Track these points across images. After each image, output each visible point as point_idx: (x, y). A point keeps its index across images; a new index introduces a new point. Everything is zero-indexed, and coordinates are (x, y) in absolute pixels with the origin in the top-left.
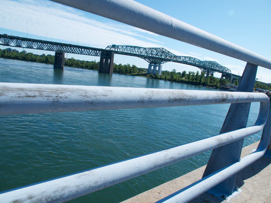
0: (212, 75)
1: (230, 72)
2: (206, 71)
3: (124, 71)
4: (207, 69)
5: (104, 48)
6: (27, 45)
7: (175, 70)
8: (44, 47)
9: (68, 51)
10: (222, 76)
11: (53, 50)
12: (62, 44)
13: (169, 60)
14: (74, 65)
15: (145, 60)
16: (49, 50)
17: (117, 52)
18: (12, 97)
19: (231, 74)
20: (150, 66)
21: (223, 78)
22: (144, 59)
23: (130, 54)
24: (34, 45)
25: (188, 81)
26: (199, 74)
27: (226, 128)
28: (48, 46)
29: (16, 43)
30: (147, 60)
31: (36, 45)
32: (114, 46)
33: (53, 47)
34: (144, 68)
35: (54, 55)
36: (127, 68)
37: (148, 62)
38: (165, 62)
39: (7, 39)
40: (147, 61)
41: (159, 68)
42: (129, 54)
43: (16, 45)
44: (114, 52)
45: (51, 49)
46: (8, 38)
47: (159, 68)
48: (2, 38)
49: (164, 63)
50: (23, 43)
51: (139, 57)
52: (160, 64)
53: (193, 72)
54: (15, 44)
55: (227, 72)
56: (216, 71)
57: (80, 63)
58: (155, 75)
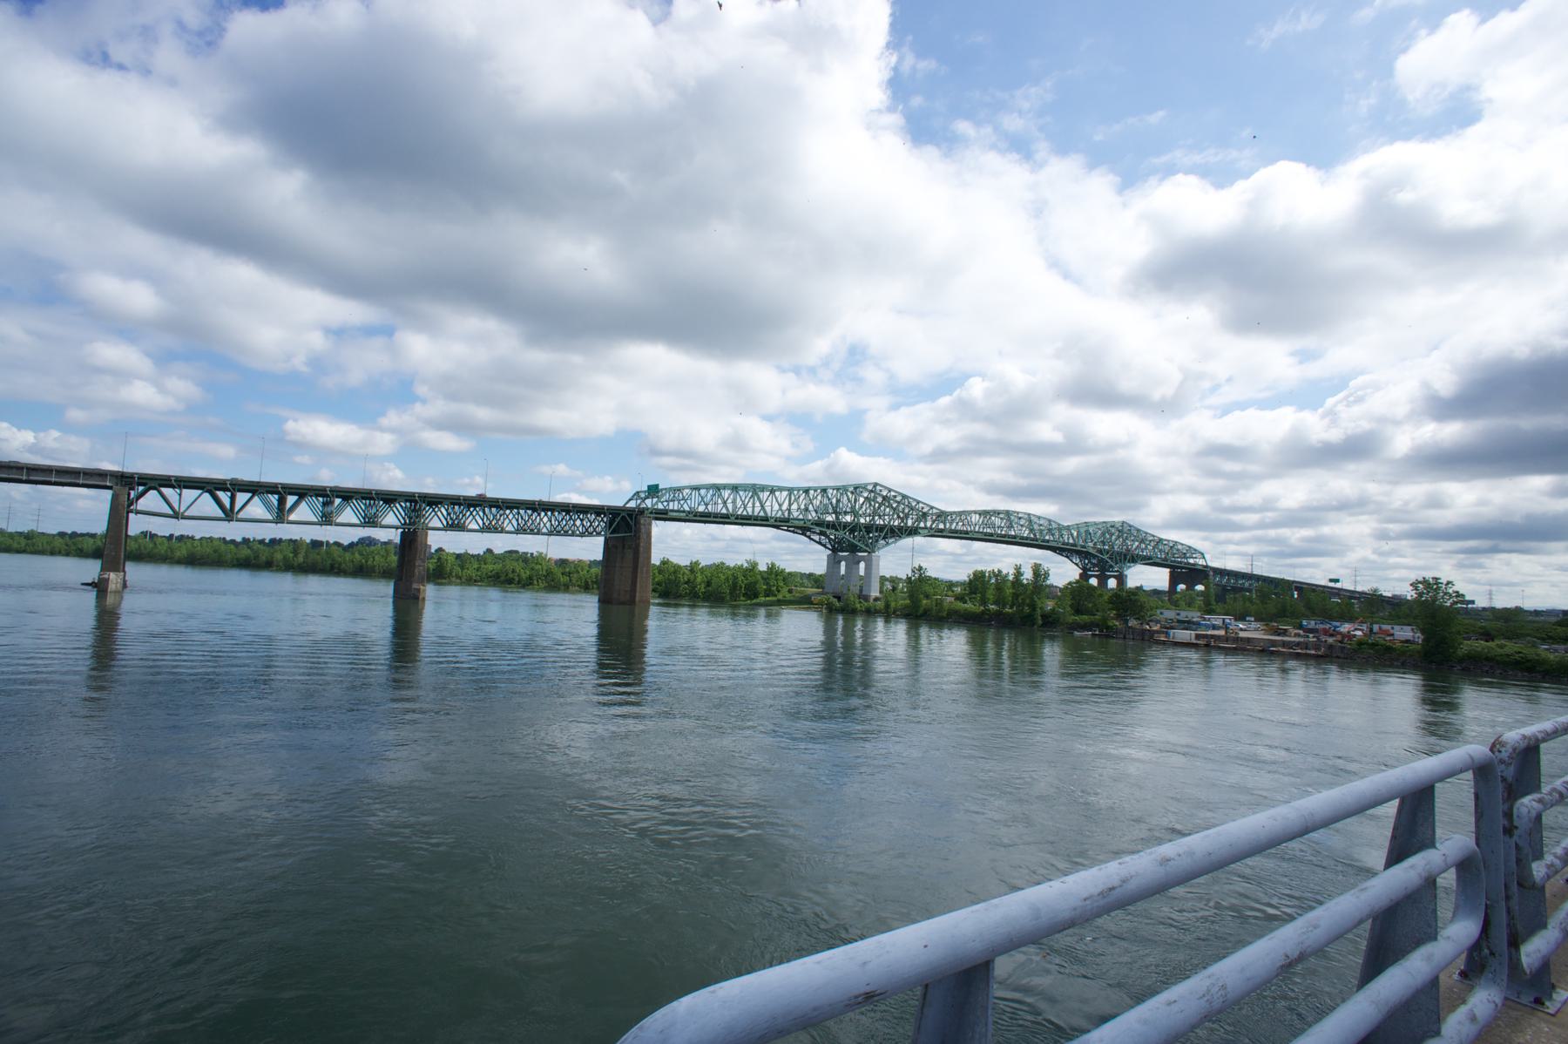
0: (1121, 579)
1: (1201, 562)
3: (702, 588)
5: (618, 502)
6: (483, 520)
7: (920, 568)
8: (542, 525)
9: (591, 529)
10: (1174, 581)
11: (573, 532)
12: (413, 495)
13: (913, 532)
14: (535, 582)
15: (809, 537)
16: (558, 534)
17: (663, 515)
19: (1207, 566)
20: (834, 562)
22: (802, 534)
23: (723, 519)
24: (507, 521)
25: (983, 613)
26: (1025, 576)
27: (1397, 854)
28: (522, 518)
29: (403, 514)
30: (816, 538)
31: (477, 518)
32: (653, 491)
33: (564, 522)
36: (736, 578)
37: (824, 546)
39: (372, 502)
40: (820, 543)
41: (868, 568)
43: (448, 523)
44: (651, 513)
45: (533, 527)
46: (375, 500)
47: (868, 568)
48: (354, 501)
50: (471, 517)
52: (871, 549)
53: (996, 570)
54: (400, 517)
55: (1189, 564)
56: (1135, 559)
57: (557, 571)
58: (839, 598)
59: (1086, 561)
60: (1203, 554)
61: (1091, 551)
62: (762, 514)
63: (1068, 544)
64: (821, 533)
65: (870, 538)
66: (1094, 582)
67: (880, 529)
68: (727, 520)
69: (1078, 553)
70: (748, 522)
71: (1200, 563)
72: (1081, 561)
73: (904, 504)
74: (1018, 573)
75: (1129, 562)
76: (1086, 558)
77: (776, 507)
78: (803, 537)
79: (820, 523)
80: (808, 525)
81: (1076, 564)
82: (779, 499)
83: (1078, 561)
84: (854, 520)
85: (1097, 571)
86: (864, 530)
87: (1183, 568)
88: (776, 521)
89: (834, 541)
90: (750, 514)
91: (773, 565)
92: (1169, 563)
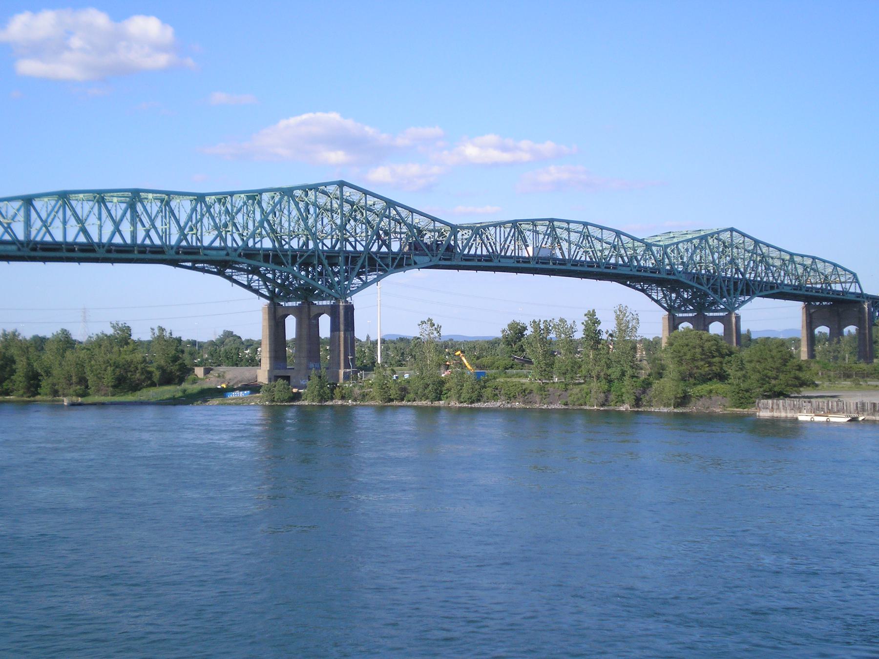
2: (686, 302)
4: (686, 287)
13: (400, 262)
15: (230, 278)
18: (37, 411)
19: (861, 295)
21: (846, 330)
22: (220, 273)
30: (243, 278)
34: (769, 336)
35: (329, 336)
37: (256, 291)
38: (747, 298)
40: (249, 287)
42: (118, 251)
49: (365, 284)
51: (175, 263)
55: (835, 292)
59: (674, 295)
60: (855, 275)
61: (683, 279)
62: (82, 239)
63: (646, 269)
64: (255, 271)
65: (336, 274)
66: (716, 328)
67: (352, 259)
68: (92, 255)
69: (661, 283)
70: (58, 254)
71: (852, 290)
72: (665, 296)
73: (388, 217)
74: (592, 321)
75: (742, 294)
76: (673, 290)
77: (108, 228)
78: (219, 277)
79: (250, 254)
80: (233, 257)
81: (657, 301)
82: (113, 213)
83: (661, 295)
84: (306, 244)
85: (691, 311)
86: (325, 262)
87: (826, 299)
88: (177, 253)
89: (273, 280)
90: (129, 241)
91: (162, 329)
92: (803, 292)
